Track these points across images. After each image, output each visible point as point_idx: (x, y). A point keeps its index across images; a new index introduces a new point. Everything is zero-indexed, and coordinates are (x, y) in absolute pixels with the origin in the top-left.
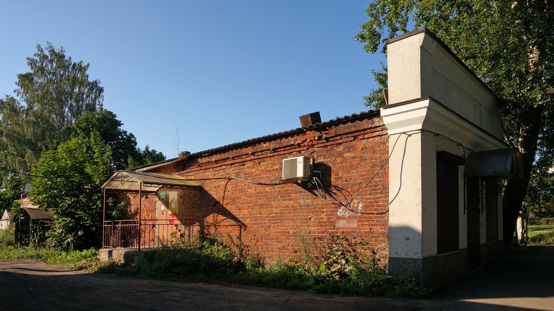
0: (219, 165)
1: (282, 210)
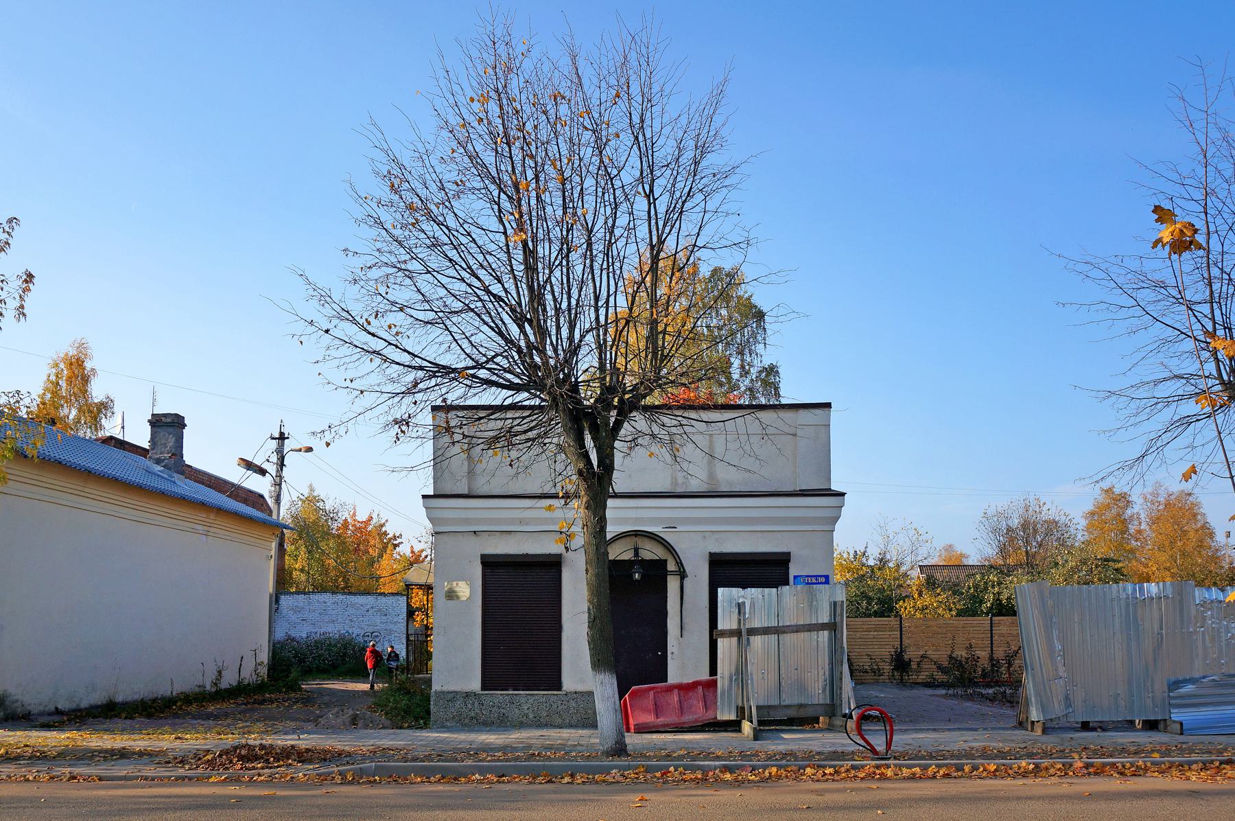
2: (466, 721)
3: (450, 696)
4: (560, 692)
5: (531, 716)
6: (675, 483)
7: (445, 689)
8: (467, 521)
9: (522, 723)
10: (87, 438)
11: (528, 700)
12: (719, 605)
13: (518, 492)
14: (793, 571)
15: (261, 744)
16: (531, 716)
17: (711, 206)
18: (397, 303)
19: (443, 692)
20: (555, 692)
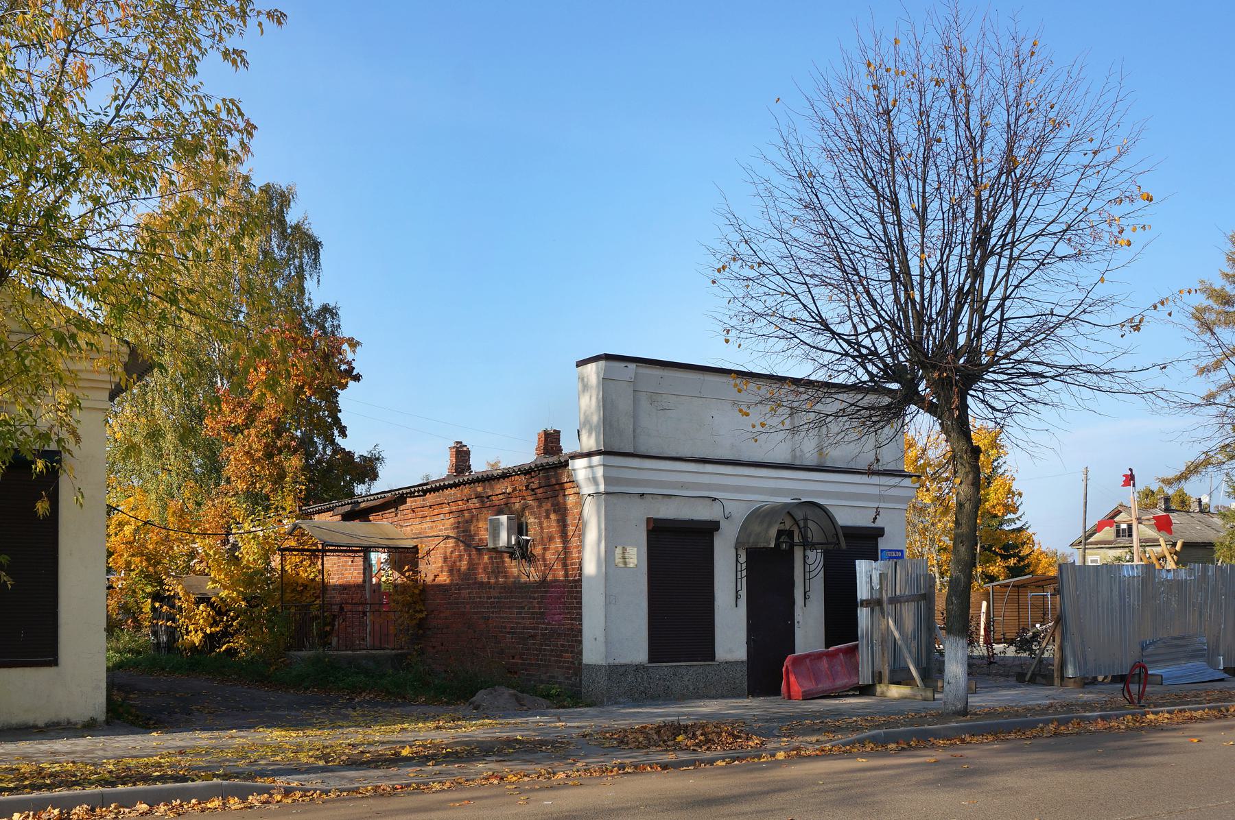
0: (436, 512)
1: (500, 593)
2: (636, 696)
3: (623, 669)
4: (714, 663)
5: (691, 688)
6: (794, 457)
7: (617, 662)
8: (637, 482)
9: (683, 695)
10: (203, 328)
11: (689, 670)
12: (858, 575)
13: (687, 454)
14: (883, 544)
15: (620, 763)
16: (691, 688)
17: (1016, 252)
18: (1081, 365)
19: (616, 666)
20: (710, 663)
